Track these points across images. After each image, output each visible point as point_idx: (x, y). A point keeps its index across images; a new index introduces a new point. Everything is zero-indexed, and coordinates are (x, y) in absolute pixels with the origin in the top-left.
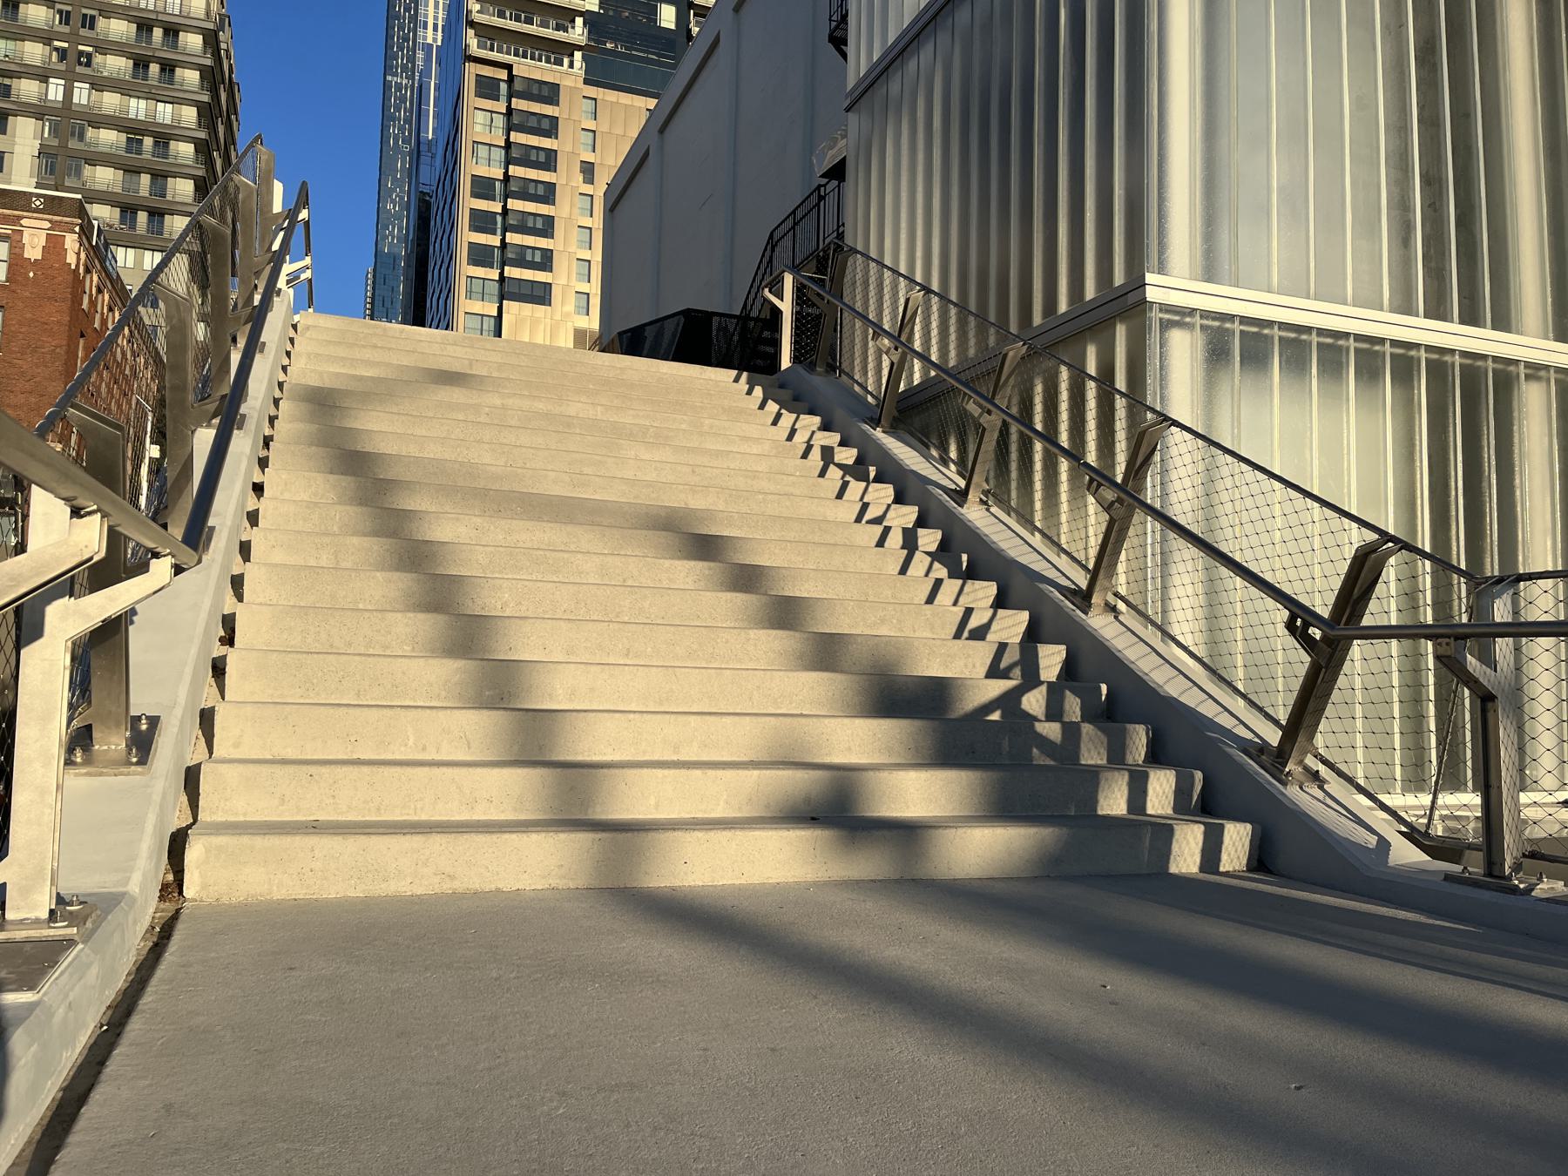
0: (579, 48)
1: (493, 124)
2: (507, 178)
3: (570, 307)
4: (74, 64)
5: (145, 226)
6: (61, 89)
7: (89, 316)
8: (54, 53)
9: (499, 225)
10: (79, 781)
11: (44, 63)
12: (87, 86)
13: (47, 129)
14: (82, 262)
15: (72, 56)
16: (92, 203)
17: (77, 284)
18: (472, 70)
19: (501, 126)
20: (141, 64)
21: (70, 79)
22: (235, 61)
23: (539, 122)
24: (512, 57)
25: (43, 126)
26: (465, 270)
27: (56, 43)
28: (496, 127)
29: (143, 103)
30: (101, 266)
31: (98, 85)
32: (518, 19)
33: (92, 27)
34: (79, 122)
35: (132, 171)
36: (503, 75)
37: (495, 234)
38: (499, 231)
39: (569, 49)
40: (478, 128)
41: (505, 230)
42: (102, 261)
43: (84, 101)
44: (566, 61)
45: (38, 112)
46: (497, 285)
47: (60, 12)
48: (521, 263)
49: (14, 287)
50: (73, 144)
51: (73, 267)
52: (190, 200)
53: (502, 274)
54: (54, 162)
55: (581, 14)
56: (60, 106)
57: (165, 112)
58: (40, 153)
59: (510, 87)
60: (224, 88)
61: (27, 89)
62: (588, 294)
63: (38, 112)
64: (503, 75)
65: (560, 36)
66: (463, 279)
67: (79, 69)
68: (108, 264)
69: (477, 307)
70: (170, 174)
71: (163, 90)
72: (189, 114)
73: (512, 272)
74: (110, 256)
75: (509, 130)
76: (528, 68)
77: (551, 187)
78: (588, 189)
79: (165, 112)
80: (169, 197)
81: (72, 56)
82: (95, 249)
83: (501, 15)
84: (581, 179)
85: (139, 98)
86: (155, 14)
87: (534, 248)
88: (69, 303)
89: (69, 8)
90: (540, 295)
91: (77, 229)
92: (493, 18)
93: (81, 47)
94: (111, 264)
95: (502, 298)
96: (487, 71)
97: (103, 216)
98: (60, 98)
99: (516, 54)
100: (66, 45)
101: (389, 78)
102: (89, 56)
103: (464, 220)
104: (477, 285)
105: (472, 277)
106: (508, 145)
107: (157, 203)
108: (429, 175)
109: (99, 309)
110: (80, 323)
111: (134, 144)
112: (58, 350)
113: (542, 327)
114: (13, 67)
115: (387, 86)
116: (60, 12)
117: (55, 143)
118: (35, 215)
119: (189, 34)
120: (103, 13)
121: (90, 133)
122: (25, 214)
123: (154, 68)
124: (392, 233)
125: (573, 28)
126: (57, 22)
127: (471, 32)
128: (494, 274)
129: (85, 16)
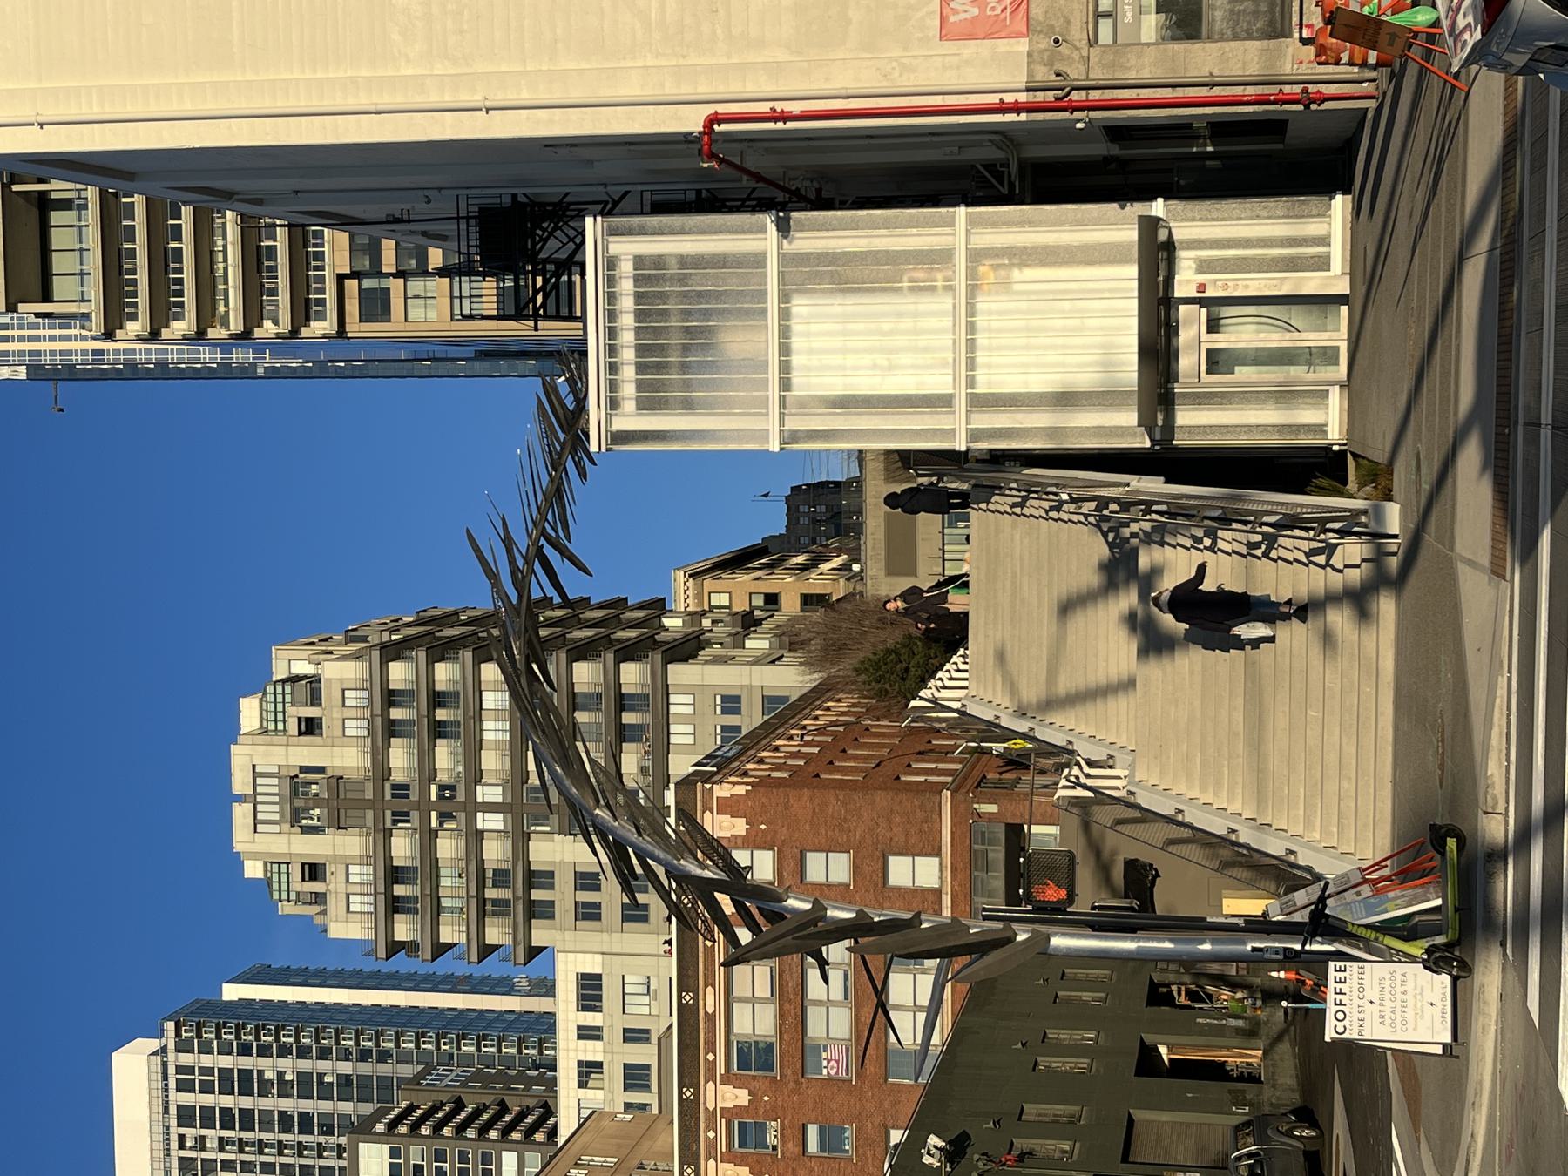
1: (422, 294)
5: (592, 714)
6: (488, 816)
7: (795, 771)
8: (445, 826)
10: (1117, 766)
12: (479, 788)
13: (538, 828)
14: (739, 779)
15: (446, 807)
16: (669, 776)
18: (355, 327)
19: (423, 283)
20: (439, 730)
22: (385, 617)
25: (535, 832)
27: (434, 823)
28: (425, 291)
29: (487, 725)
30: (734, 761)
31: (475, 776)
33: (407, 787)
34: (525, 794)
36: (352, 285)
40: (432, 315)
45: (520, 839)
47: (395, 822)
49: (779, 842)
51: (749, 788)
52: (647, 668)
56: (509, 816)
58: (571, 834)
60: (438, 631)
61: (495, 852)
63: (520, 839)
64: (352, 285)
67: (461, 797)
68: (730, 754)
70: (570, 690)
71: (468, 704)
75: (425, 273)
80: (600, 689)
82: (720, 767)
83: (273, 292)
85: (481, 730)
86: (378, 896)
88: (788, 790)
89: (388, 813)
91: (708, 786)
92: (280, 305)
93: (434, 797)
94: (728, 751)
96: (352, 307)
97: (635, 761)
98: (500, 816)
100: (434, 814)
102: (442, 788)
107: (609, 702)
109: (782, 761)
110: (806, 777)
114: (473, 868)
116: (395, 822)
117: (555, 819)
119: (390, 678)
120: (432, 778)
123: (441, 714)
126: (408, 825)
127: (305, 332)
129: (393, 796)
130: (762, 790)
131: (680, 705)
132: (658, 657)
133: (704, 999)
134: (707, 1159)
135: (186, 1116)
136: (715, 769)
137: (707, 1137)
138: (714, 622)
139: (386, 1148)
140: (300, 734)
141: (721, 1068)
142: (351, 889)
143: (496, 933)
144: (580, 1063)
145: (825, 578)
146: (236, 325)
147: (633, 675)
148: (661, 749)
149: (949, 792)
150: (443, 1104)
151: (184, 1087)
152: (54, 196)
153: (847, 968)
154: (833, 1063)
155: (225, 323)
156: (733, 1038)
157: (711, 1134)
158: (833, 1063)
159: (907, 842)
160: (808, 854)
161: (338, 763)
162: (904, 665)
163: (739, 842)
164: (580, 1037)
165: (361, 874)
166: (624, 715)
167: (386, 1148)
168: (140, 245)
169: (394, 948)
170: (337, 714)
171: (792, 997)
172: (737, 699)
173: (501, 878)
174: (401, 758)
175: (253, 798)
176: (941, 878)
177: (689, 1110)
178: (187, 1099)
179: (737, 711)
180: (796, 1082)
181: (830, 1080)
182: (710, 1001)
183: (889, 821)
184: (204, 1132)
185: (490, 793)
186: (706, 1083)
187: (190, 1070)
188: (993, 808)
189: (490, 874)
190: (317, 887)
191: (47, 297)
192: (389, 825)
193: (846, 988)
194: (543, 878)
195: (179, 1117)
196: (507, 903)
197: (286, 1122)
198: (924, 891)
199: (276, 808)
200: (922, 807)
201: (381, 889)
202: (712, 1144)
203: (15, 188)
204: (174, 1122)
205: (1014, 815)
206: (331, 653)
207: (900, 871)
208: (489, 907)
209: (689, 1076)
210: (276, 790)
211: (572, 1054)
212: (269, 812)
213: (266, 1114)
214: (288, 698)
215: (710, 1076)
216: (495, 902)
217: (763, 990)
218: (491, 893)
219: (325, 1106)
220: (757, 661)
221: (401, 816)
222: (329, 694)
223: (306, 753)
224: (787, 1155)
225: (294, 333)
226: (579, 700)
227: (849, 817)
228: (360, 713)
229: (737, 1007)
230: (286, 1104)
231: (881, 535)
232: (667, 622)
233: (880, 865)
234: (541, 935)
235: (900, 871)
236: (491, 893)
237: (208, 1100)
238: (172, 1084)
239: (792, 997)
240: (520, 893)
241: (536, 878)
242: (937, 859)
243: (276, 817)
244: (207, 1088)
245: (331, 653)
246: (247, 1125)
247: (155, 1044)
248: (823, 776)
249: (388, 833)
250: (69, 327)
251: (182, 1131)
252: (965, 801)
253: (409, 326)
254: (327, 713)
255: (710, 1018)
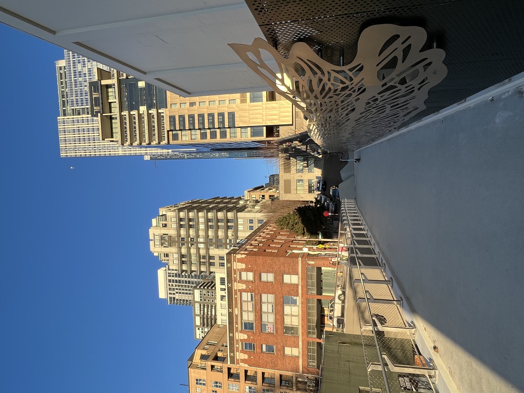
0: (157, 111)
2: (199, 129)
3: (234, 106)
4: (194, 242)
6: (201, 245)
7: (260, 248)
9: (213, 130)
11: (195, 249)
12: (199, 239)
13: (211, 247)
15: (192, 243)
17: (251, 254)
18: (171, 142)
20: (190, 226)
21: (198, 243)
23: (181, 121)
24: (165, 131)
26: (228, 139)
27: (190, 246)
29: (200, 225)
31: (198, 236)
32: (154, 130)
33: (184, 238)
35: (218, 227)
36: (170, 133)
37: (216, 131)
38: (215, 130)
39: (158, 114)
40: (187, 139)
41: (215, 128)
42: (243, 245)
43: (203, 239)
44: (162, 114)
45: (208, 249)
46: (231, 129)
47: (182, 246)
48: (223, 122)
49: (254, 270)
50: (214, 241)
51: (246, 256)
53: (227, 128)
54: (219, 244)
55: (148, 111)
57: (202, 220)
59: (174, 131)
62: (229, 100)
63: (208, 249)
64: (170, 133)
65: (155, 117)
66: (231, 139)
67: (195, 241)
68: (243, 243)
69: (239, 134)
72: (201, 214)
73: (227, 125)
74: (241, 242)
76: (167, 126)
77: (199, 115)
78: (197, 104)
79: (202, 220)
81: (192, 243)
83: (154, 135)
84: (195, 106)
87: (218, 119)
89: (180, 244)
90: (232, 116)
91: (235, 255)
93: (189, 241)
95: (235, 127)
96: (171, 137)
98: (203, 245)
99: (164, 129)
100: (190, 244)
101: (186, 158)
102: (191, 239)
103: (213, 141)
104: (232, 135)
105: (230, 137)
106: (190, 129)
108: (205, 150)
111: (211, 227)
112: (271, 259)
113: (241, 114)
115: (188, 158)
116: (182, 246)
118: (232, 266)
121: (210, 237)
122: (233, 268)
123: (191, 223)
124: (224, 154)
125: (152, 113)
127: (161, 143)
128: (228, 130)
129: (181, 240)
130: (249, 256)
131: (240, 221)
132: (235, 211)
133: (235, 311)
134: (236, 352)
135: (170, 281)
136: (238, 248)
137: (236, 346)
138: (250, 202)
139: (199, 291)
140: (163, 227)
141: (240, 329)
142: (174, 259)
143: (203, 269)
144: (221, 296)
145: (272, 192)
146: (147, 142)
147: (230, 215)
148: (236, 231)
149: (300, 258)
150: (210, 282)
151: (169, 276)
152: (113, 116)
153: (273, 304)
154: (269, 329)
155: (145, 142)
156: (242, 321)
157: (237, 346)
158: (269, 329)
159: (289, 271)
160: (262, 274)
161: (170, 233)
162: (288, 221)
163: (243, 270)
164: (221, 290)
165: (176, 256)
166: (228, 223)
167: (199, 291)
168: (128, 126)
169: (183, 271)
170: (170, 223)
171: (258, 311)
172: (252, 220)
173: (204, 257)
174: (183, 232)
175: (154, 240)
176: (298, 281)
177: (232, 339)
178: (170, 278)
179: (252, 223)
180: (260, 333)
181: (269, 333)
182: (236, 311)
183: (284, 266)
184: (173, 283)
185: (201, 240)
186: (236, 332)
187: (170, 273)
188: (313, 263)
189: (202, 256)
190: (167, 258)
191: (112, 137)
192: (181, 246)
193: (273, 309)
194: (212, 258)
195: (169, 281)
196: (205, 262)
197: (186, 282)
198: (294, 285)
199: (159, 242)
200: (293, 262)
201: (179, 259)
202: (237, 348)
203: (103, 115)
204: (168, 282)
205: (319, 264)
206: (170, 210)
207: (287, 279)
208: (202, 263)
209: (231, 330)
210: (158, 238)
211: (219, 294)
212: (158, 243)
213: (183, 281)
214: (161, 219)
215: (237, 331)
216: (203, 262)
217: (250, 309)
218: (202, 260)
219: (192, 280)
220: (257, 212)
221: (183, 244)
222: (168, 219)
223: (164, 231)
224: (257, 352)
225: (159, 143)
226: (220, 220)
227: (273, 264)
228: (174, 223)
229: (243, 313)
230: (186, 279)
231: (283, 185)
232: (240, 202)
233: (282, 277)
234: (212, 269)
235: (287, 279)
236: (202, 260)
237: (173, 278)
238: (167, 276)
239: (258, 311)
240: (208, 261)
241: (211, 258)
242: (297, 276)
243: (159, 244)
244: (173, 276)
245: (170, 210)
246: (180, 282)
247: (164, 268)
248: (267, 251)
249: (180, 248)
250: (136, 149)
251: (169, 283)
252: (305, 261)
253: (183, 141)
254: (168, 223)
255: (237, 316)
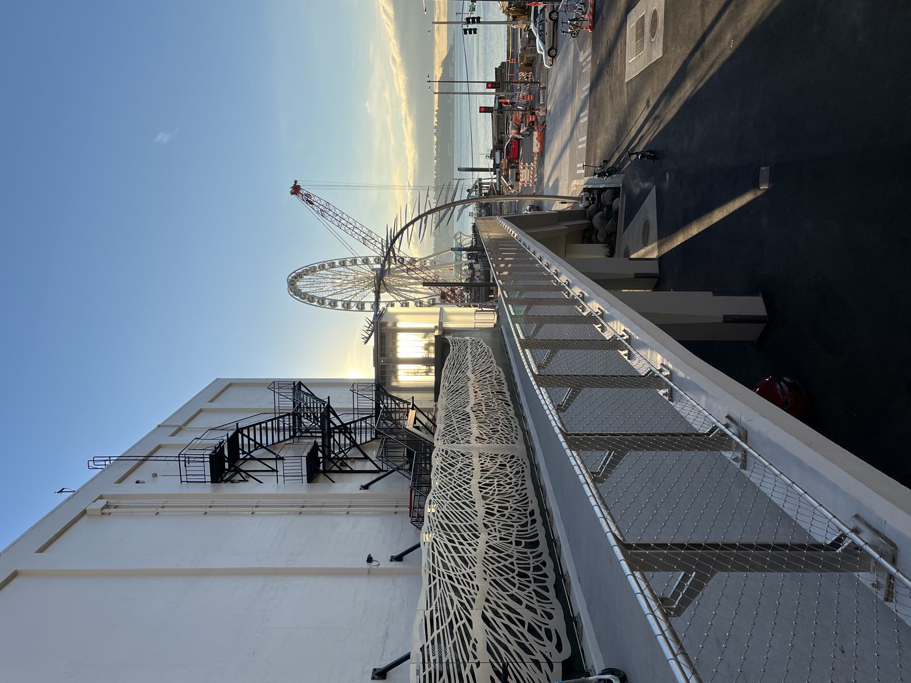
40: (596, 192)
